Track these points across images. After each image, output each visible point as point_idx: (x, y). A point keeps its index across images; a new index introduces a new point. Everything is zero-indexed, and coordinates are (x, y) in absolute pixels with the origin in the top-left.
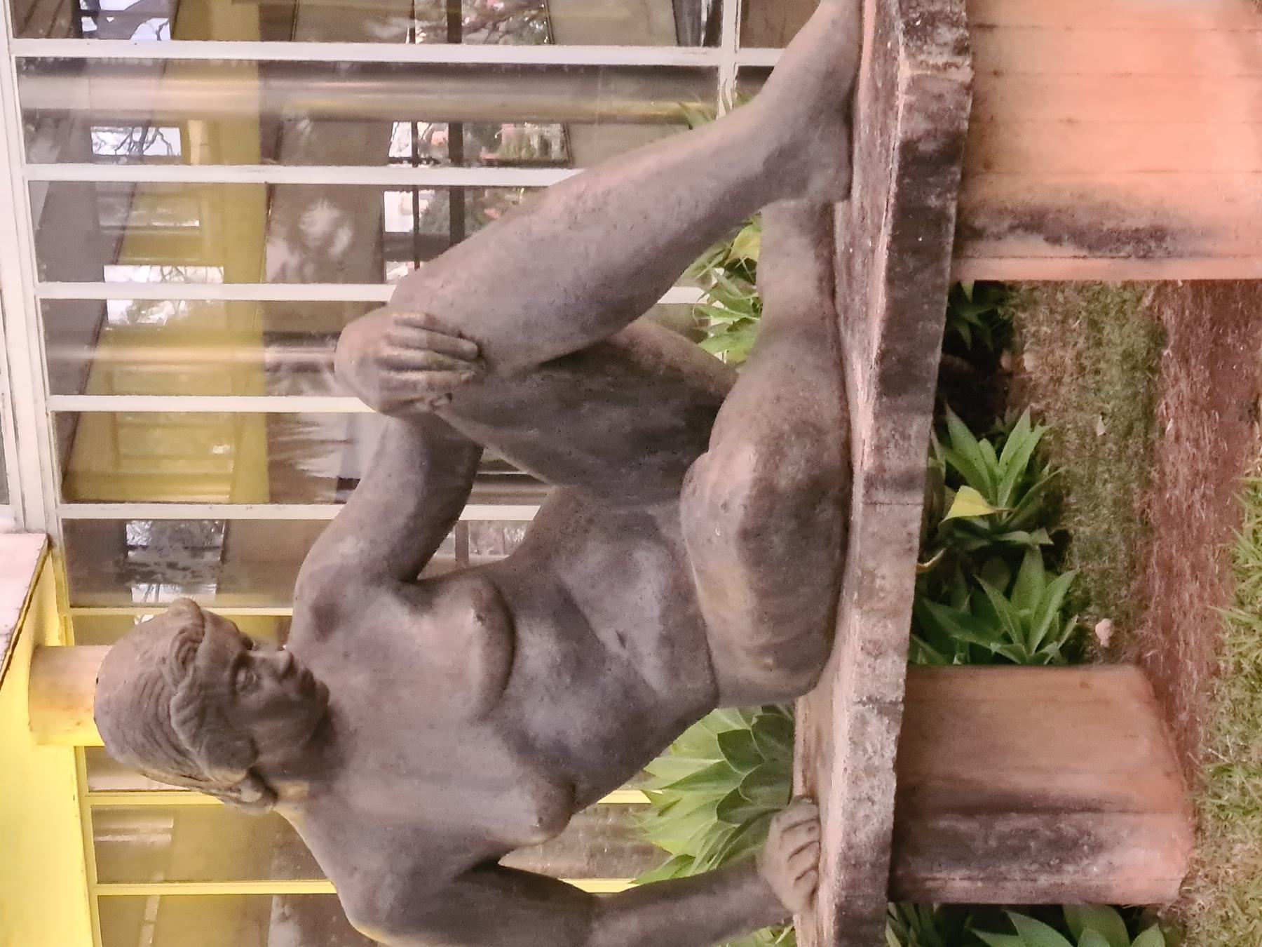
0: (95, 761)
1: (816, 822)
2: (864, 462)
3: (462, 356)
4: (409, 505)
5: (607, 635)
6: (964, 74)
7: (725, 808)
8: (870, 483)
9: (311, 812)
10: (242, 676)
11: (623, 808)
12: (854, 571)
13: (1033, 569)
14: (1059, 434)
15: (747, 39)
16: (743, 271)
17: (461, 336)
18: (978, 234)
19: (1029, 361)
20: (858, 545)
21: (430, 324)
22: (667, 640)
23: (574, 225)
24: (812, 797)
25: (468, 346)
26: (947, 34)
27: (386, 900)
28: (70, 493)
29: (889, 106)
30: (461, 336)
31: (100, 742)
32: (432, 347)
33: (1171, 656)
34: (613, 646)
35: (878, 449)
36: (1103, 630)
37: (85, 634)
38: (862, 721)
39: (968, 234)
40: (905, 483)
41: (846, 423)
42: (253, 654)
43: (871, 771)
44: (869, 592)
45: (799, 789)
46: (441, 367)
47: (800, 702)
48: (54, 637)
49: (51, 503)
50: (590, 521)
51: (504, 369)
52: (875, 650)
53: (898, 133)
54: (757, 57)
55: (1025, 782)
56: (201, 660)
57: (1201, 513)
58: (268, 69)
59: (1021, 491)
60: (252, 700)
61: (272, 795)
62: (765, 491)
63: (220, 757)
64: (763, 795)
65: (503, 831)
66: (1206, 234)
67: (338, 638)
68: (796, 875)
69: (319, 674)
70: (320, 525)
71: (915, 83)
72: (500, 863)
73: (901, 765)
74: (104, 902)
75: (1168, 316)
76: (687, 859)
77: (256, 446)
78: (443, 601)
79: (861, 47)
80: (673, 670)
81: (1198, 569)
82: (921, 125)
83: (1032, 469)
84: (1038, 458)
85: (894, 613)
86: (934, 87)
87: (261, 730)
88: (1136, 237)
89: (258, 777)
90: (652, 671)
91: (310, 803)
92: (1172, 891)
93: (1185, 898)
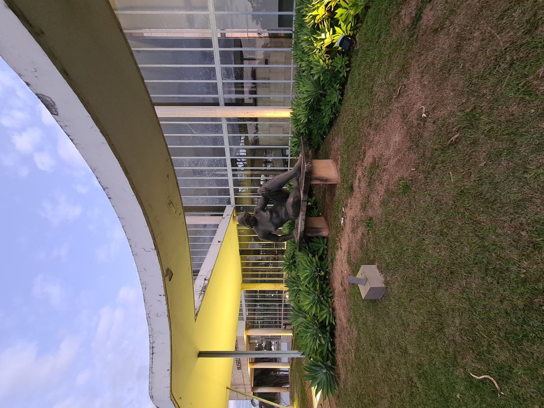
0: (238, 225)
1: (297, 230)
2: (302, 199)
4: (263, 203)
5: (280, 214)
6: (311, 166)
7: (289, 229)
9: (255, 229)
11: (280, 229)
13: (315, 209)
14: (317, 198)
16: (291, 185)
18: (312, 180)
19: (314, 192)
20: (301, 206)
21: (265, 188)
22: (285, 214)
23: (278, 179)
24: (297, 228)
26: (309, 162)
27: (262, 236)
28: (236, 204)
29: (304, 169)
31: (238, 224)
32: (265, 190)
33: (327, 216)
34: (281, 215)
35: (303, 198)
36: (321, 214)
37: (237, 215)
38: (301, 221)
39: (311, 180)
40: (305, 201)
41: (300, 196)
43: (302, 225)
44: (302, 210)
45: (296, 227)
47: (296, 220)
48: (235, 215)
51: (271, 191)
52: (303, 215)
53: (305, 171)
54: (291, 168)
55: (315, 226)
56: (246, 216)
57: (329, 203)
58: (252, 170)
59: (313, 203)
60: (251, 219)
61: (252, 227)
62: (293, 202)
63: (248, 224)
64: (293, 228)
65: (271, 230)
66: (331, 180)
67: (258, 214)
69: (256, 217)
70: (255, 206)
71: (307, 167)
73: (305, 225)
74: (239, 236)
75: (326, 188)
76: (286, 233)
77: (250, 200)
78: (266, 211)
80: (285, 217)
81: (329, 208)
82: (307, 170)
83: (314, 201)
84: (315, 200)
85: (304, 212)
86: (308, 167)
87: (251, 222)
88: (325, 180)
89: (251, 226)
90: (284, 217)
91: (255, 228)
92: (327, 235)
93: (328, 236)
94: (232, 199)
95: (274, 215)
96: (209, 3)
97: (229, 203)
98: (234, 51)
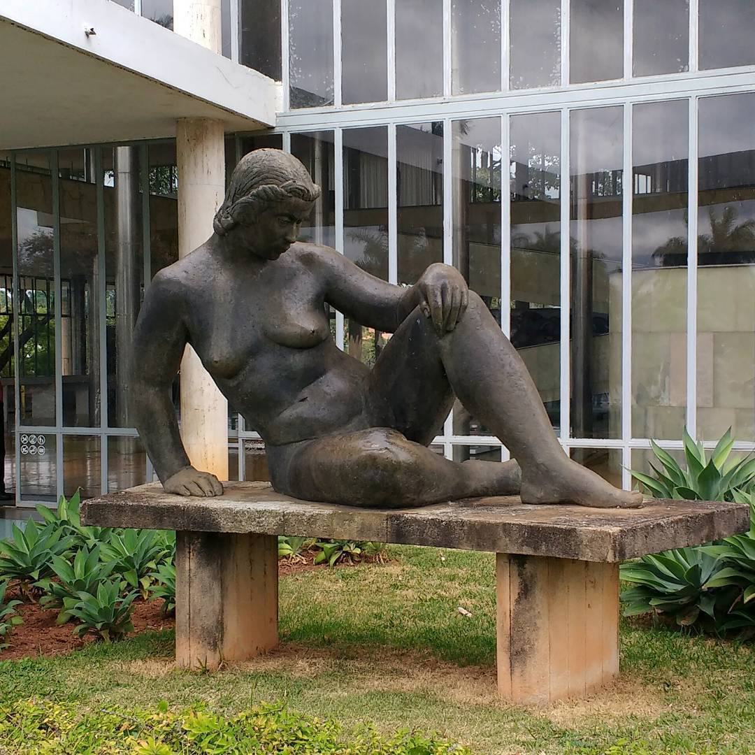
2: (409, 514)
3: (448, 323)
8: (398, 518)
10: (286, 219)
12: (351, 511)
15: (68, 438)
17: (457, 322)
25: (453, 325)
30: (457, 322)
34: (301, 396)
42: (295, 224)
46: (443, 313)
49: (290, 129)
50: (357, 383)
68: (186, 485)
72: (188, 345)
79: (599, 507)
80: (290, 424)
90: (288, 414)
94: (322, 118)
95: (298, 361)
96: (361, 174)
97: (300, 98)
98: (699, 206)
